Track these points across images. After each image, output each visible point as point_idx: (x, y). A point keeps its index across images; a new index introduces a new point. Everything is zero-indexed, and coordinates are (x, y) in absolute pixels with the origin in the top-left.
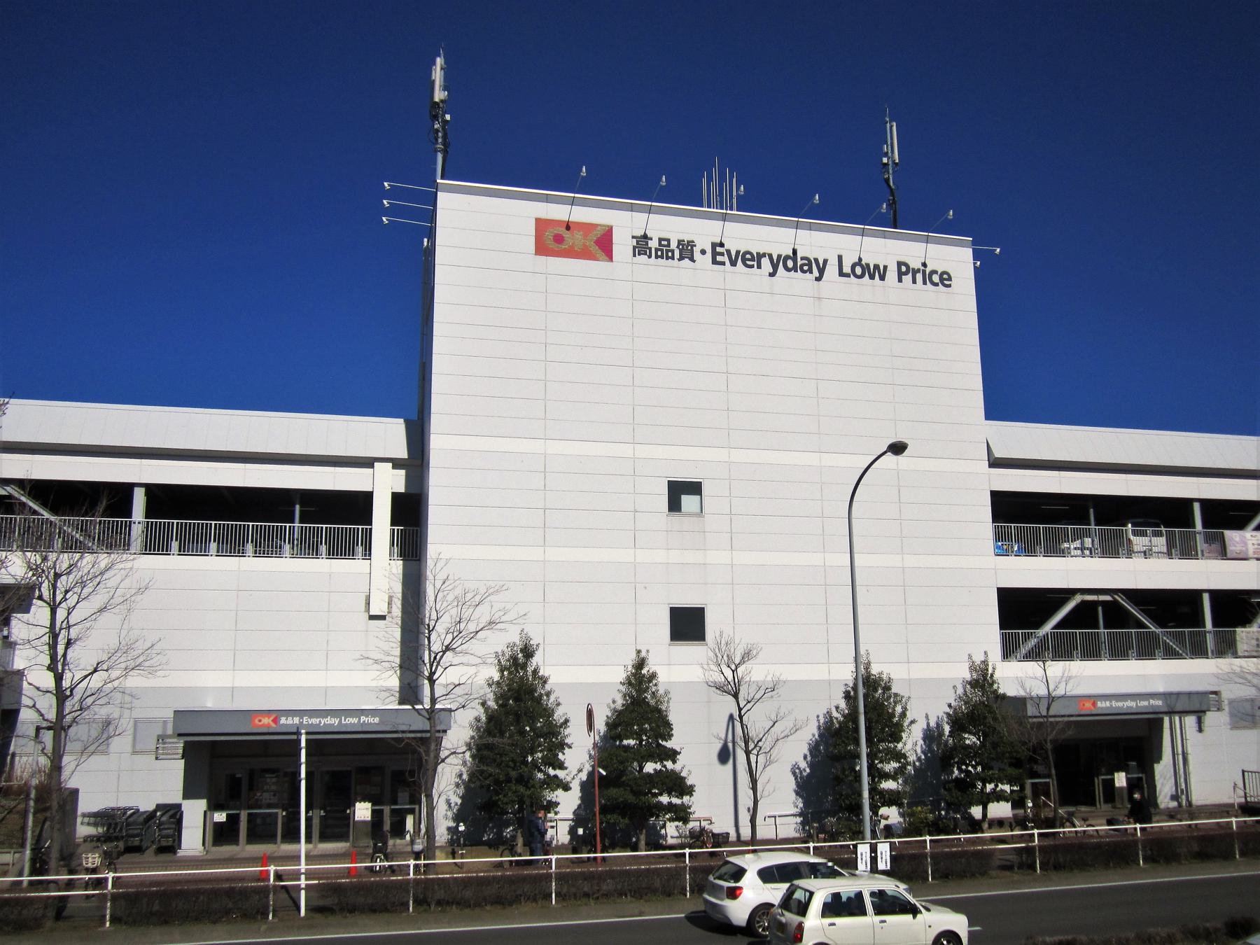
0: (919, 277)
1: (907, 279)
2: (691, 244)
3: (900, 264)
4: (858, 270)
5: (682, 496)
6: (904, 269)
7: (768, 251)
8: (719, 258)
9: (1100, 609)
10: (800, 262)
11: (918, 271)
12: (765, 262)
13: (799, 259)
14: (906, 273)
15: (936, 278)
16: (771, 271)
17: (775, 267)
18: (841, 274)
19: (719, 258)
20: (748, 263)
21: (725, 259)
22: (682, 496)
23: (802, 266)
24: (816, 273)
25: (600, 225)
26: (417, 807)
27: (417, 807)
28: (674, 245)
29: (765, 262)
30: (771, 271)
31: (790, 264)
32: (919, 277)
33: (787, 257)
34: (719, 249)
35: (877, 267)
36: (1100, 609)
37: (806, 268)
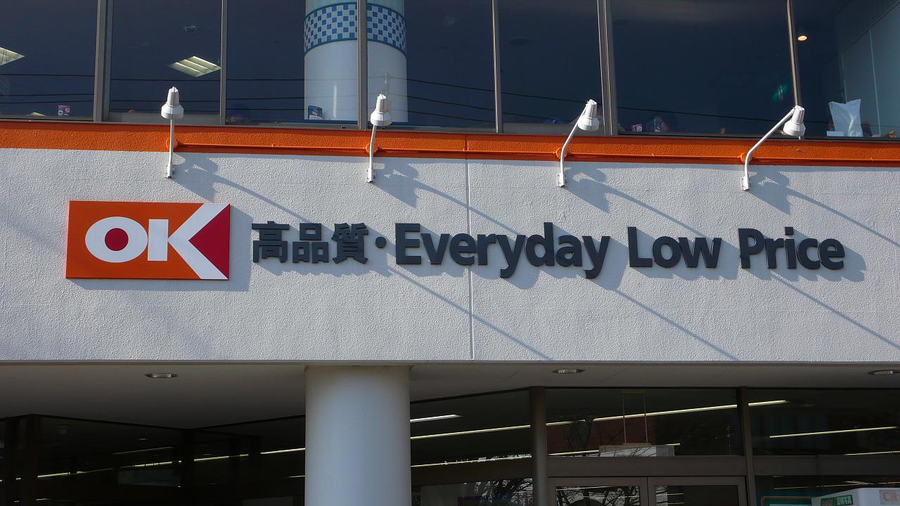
0: (781, 255)
1: (760, 260)
2: (361, 230)
3: (745, 234)
4: (667, 253)
5: (166, 260)
6: (752, 242)
7: (499, 231)
8: (411, 252)
9: (529, 456)
10: (557, 247)
11: (780, 243)
12: (495, 253)
13: (556, 242)
14: (756, 251)
15: (813, 255)
16: (505, 266)
17: (512, 259)
18: (83, 214)
19: (411, 252)
20: (465, 256)
21: (421, 252)
22: (166, 260)
23: (563, 251)
24: (588, 264)
25: (21, 417)
26: (220, 119)
27: (220, 119)
28: (327, 237)
29: (495, 253)
30: (505, 266)
31: (540, 251)
32: (781, 255)
33: (535, 240)
34: (411, 236)
35: (701, 242)
36: (529, 456)
37: (569, 256)
